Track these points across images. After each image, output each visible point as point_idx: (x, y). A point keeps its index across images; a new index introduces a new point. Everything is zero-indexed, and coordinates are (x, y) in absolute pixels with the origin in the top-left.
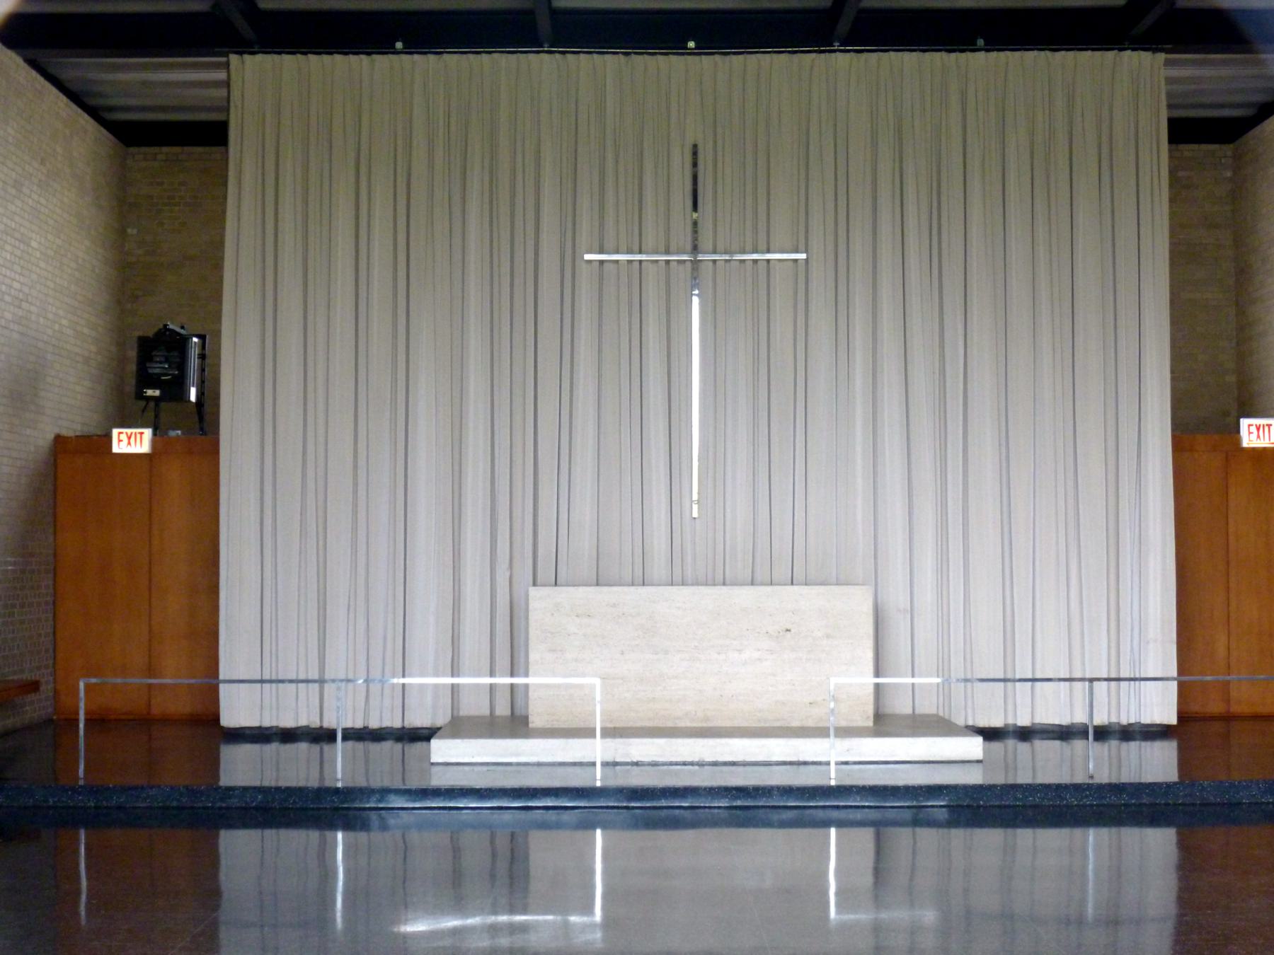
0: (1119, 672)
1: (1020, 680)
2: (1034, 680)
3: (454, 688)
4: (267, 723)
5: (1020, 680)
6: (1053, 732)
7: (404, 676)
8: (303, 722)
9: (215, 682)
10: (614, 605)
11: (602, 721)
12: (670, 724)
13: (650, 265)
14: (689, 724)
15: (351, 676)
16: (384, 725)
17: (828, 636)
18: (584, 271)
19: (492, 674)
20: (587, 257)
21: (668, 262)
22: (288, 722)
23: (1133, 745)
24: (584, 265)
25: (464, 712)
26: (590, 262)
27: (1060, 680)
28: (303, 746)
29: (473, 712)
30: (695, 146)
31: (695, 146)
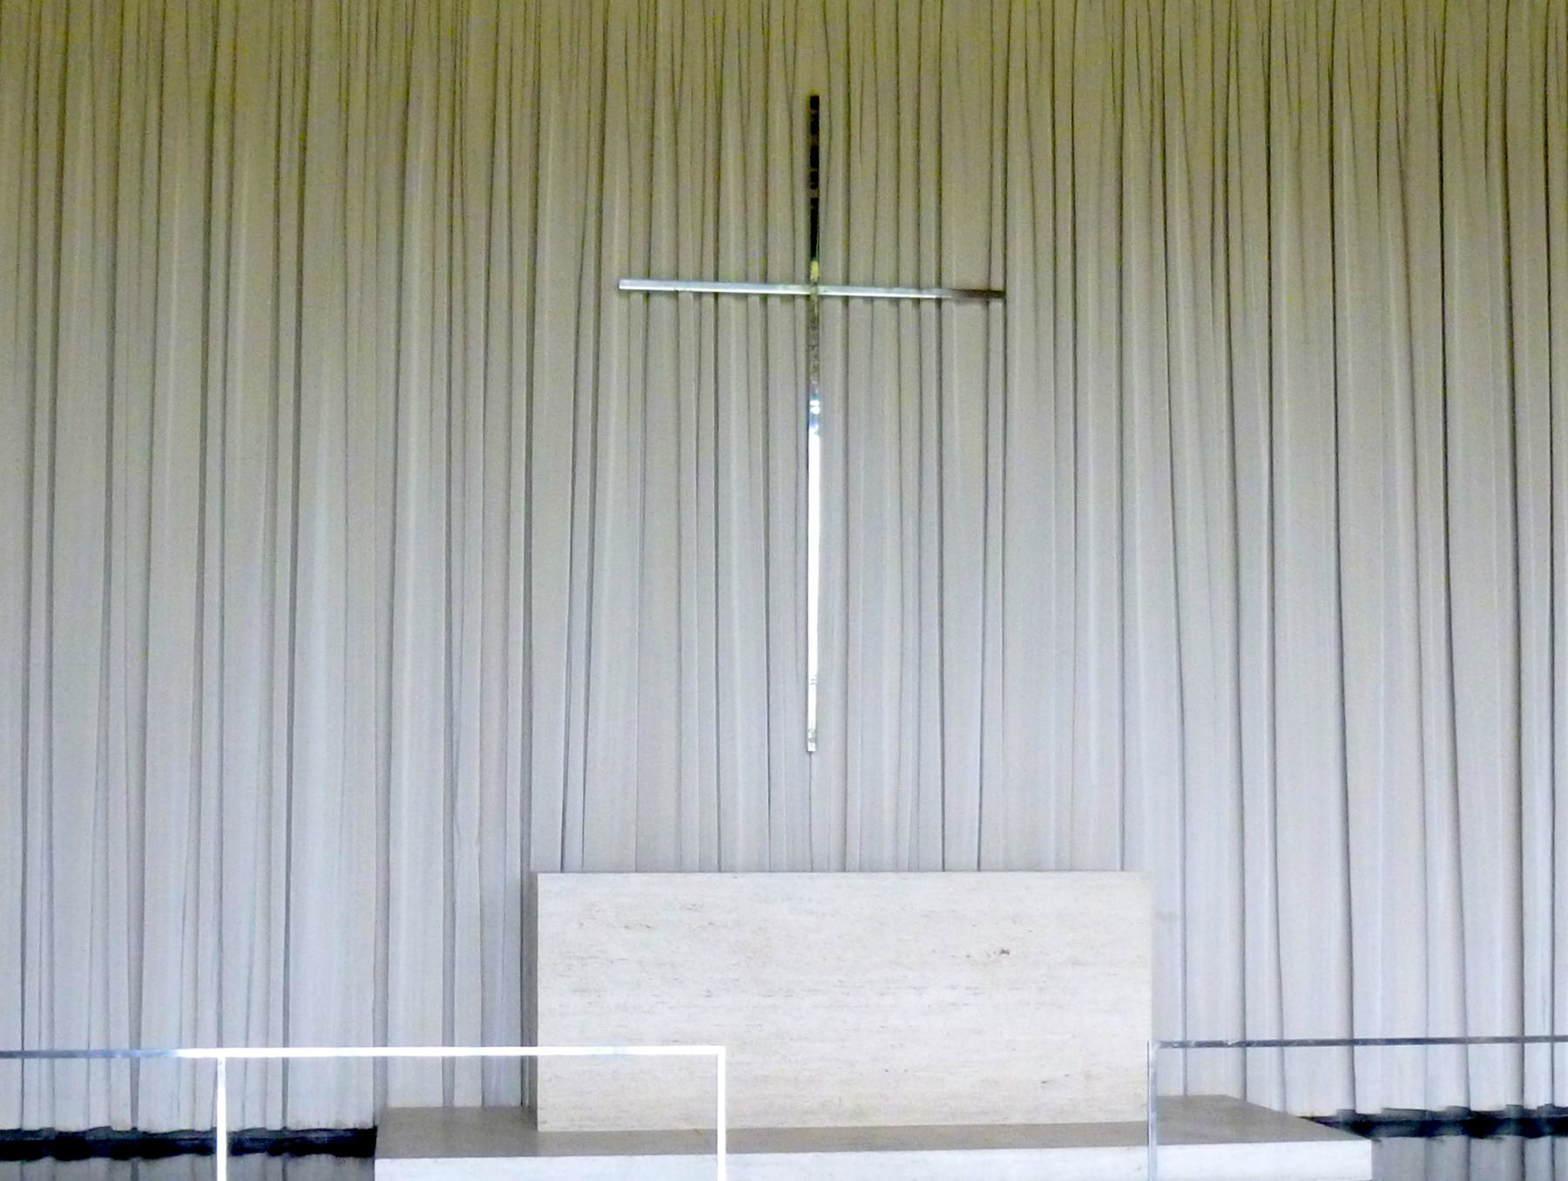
0: (1282, 1033)
1: (1200, 1045)
2: (1282, 1044)
3: (382, 1065)
4: (32, 1124)
5: (1200, 1045)
6: (1408, 1122)
7: (286, 1044)
8: (98, 1121)
9: (1153, 1140)
10: (694, 908)
11: (729, 1119)
12: (792, 1123)
13: (732, 302)
14: (829, 1123)
15: (997, 285)
16: (248, 1126)
17: (1075, 963)
18: (615, 308)
19: (449, 1040)
20: (626, 285)
21: (765, 297)
22: (72, 1122)
23: (1544, 1142)
24: (615, 298)
25: (395, 1102)
26: (629, 292)
27: (1375, 1042)
28: (99, 1165)
29: (412, 1102)
30: (814, 102)
31: (814, 102)
